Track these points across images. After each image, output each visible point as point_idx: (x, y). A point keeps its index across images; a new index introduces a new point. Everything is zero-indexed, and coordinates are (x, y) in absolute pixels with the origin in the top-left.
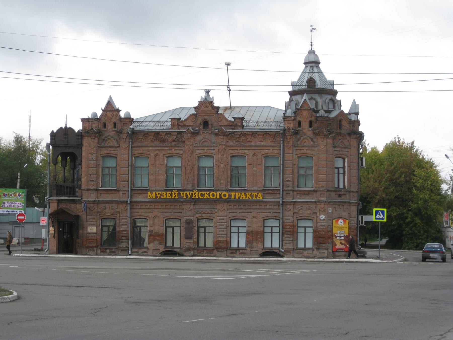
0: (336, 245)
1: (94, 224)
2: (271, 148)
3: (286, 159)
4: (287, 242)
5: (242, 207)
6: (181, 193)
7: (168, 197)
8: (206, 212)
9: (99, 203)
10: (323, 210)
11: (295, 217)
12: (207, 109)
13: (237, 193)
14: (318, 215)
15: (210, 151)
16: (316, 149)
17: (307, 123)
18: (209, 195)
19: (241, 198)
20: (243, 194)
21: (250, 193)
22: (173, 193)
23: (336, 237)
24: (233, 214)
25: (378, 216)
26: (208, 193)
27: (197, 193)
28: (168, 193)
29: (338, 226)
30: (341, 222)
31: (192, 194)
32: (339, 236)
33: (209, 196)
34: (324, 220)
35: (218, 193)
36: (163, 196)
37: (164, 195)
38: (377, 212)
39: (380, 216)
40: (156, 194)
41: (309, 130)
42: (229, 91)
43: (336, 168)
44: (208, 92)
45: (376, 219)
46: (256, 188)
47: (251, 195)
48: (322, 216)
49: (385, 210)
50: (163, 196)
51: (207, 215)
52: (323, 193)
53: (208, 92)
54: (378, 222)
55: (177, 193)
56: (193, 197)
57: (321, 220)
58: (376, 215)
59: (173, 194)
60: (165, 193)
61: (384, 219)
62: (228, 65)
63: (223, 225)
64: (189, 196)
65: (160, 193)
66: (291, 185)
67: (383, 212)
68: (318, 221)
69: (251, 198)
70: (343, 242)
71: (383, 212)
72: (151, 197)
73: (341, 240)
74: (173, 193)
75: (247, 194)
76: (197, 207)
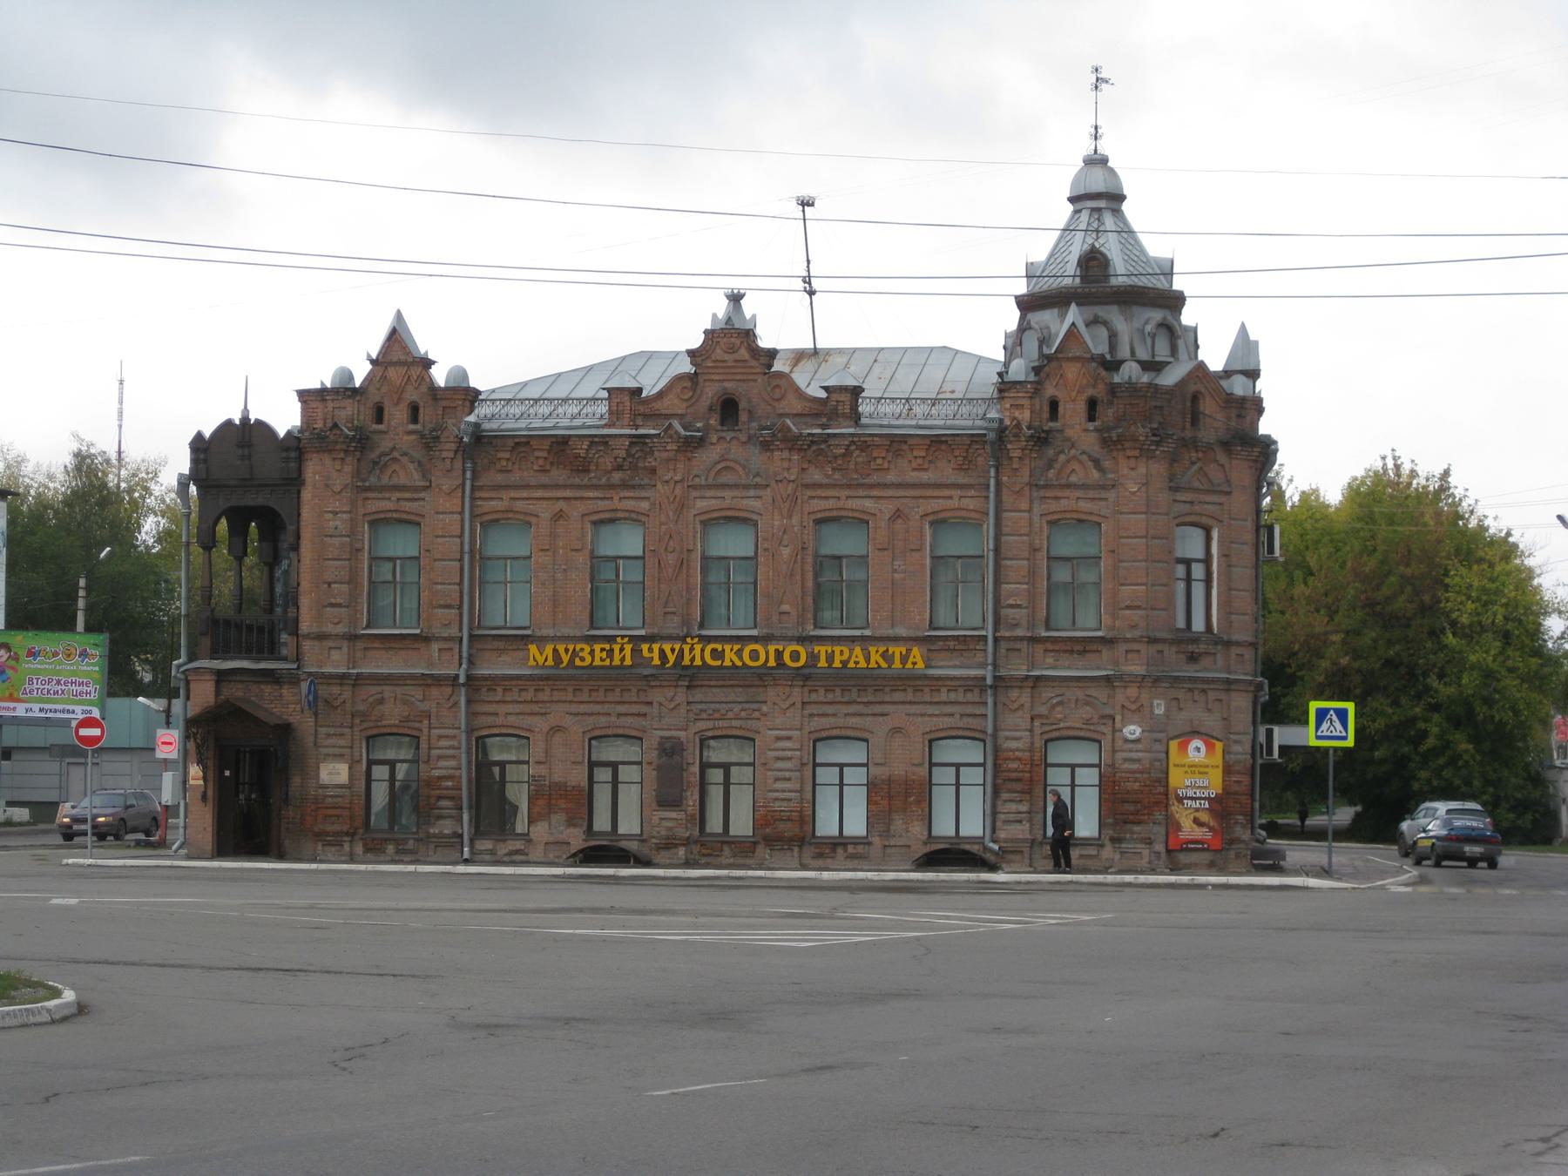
0: (1179, 828)
1: (342, 756)
2: (956, 493)
3: (1005, 530)
4: (1011, 817)
5: (854, 695)
6: (645, 647)
7: (597, 662)
8: (730, 715)
9: (358, 681)
10: (1134, 707)
11: (1038, 731)
12: (736, 356)
13: (837, 649)
14: (1118, 725)
15: (745, 502)
16: (1111, 495)
17: (1081, 407)
18: (739, 653)
19: (851, 665)
20: (858, 650)
21: (882, 649)
22: (617, 648)
23: (1180, 800)
24: (824, 720)
25: (1325, 726)
26: (736, 647)
27: (698, 647)
28: (597, 647)
29: (1187, 761)
30: (1198, 749)
31: (681, 650)
32: (1191, 798)
33: (741, 658)
34: (1137, 741)
35: (772, 649)
36: (583, 659)
37: (585, 654)
38: (1322, 715)
39: (1333, 726)
40: (555, 650)
41: (1086, 430)
42: (811, 293)
43: (1180, 561)
44: (735, 299)
45: (1318, 738)
46: (901, 631)
47: (884, 655)
48: (1132, 727)
49: (1350, 706)
50: (583, 659)
51: (736, 723)
52: (1135, 646)
53: (735, 299)
54: (1327, 749)
55: (628, 648)
56: (686, 661)
57: (1126, 741)
58: (1317, 729)
59: (617, 651)
60: (588, 649)
61: (1345, 738)
62: (806, 203)
63: (789, 759)
64: (672, 658)
65: (571, 647)
66: (1024, 622)
67: (1342, 714)
68: (1119, 743)
69: (884, 665)
70: (1204, 817)
71: (1342, 714)
72: (541, 660)
73: (1197, 810)
74: (617, 648)
75: (872, 650)
76: (698, 695)
